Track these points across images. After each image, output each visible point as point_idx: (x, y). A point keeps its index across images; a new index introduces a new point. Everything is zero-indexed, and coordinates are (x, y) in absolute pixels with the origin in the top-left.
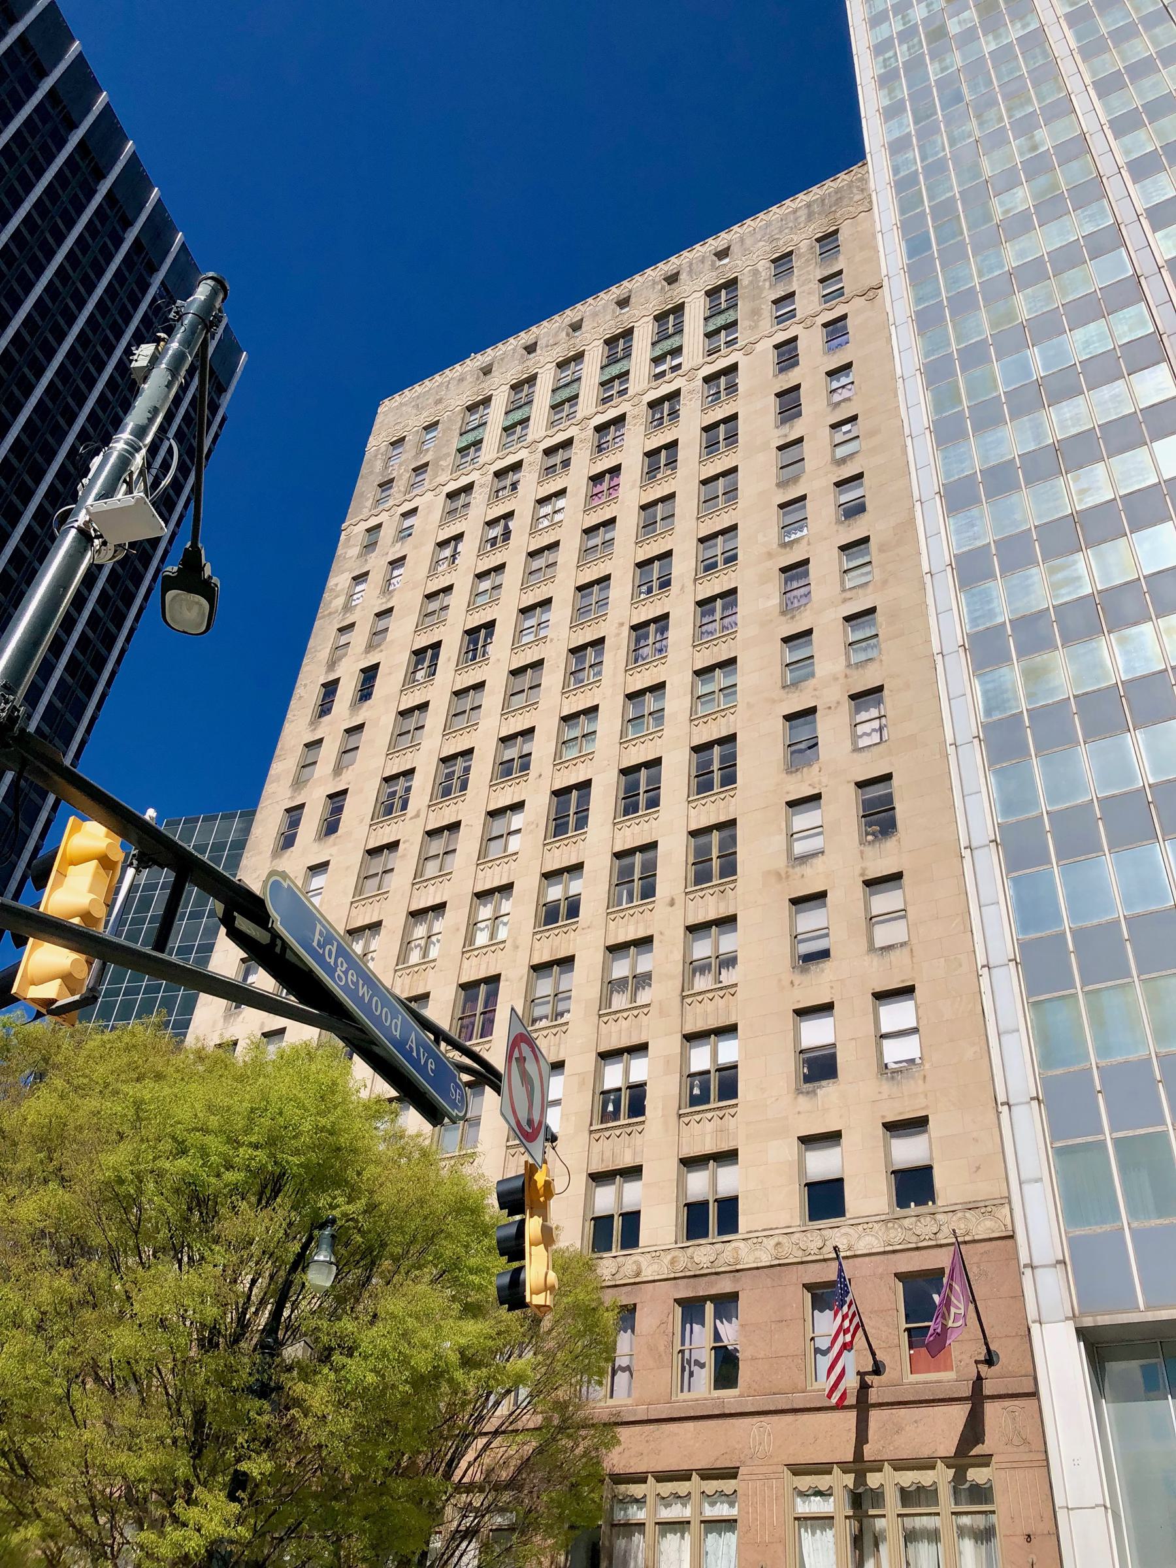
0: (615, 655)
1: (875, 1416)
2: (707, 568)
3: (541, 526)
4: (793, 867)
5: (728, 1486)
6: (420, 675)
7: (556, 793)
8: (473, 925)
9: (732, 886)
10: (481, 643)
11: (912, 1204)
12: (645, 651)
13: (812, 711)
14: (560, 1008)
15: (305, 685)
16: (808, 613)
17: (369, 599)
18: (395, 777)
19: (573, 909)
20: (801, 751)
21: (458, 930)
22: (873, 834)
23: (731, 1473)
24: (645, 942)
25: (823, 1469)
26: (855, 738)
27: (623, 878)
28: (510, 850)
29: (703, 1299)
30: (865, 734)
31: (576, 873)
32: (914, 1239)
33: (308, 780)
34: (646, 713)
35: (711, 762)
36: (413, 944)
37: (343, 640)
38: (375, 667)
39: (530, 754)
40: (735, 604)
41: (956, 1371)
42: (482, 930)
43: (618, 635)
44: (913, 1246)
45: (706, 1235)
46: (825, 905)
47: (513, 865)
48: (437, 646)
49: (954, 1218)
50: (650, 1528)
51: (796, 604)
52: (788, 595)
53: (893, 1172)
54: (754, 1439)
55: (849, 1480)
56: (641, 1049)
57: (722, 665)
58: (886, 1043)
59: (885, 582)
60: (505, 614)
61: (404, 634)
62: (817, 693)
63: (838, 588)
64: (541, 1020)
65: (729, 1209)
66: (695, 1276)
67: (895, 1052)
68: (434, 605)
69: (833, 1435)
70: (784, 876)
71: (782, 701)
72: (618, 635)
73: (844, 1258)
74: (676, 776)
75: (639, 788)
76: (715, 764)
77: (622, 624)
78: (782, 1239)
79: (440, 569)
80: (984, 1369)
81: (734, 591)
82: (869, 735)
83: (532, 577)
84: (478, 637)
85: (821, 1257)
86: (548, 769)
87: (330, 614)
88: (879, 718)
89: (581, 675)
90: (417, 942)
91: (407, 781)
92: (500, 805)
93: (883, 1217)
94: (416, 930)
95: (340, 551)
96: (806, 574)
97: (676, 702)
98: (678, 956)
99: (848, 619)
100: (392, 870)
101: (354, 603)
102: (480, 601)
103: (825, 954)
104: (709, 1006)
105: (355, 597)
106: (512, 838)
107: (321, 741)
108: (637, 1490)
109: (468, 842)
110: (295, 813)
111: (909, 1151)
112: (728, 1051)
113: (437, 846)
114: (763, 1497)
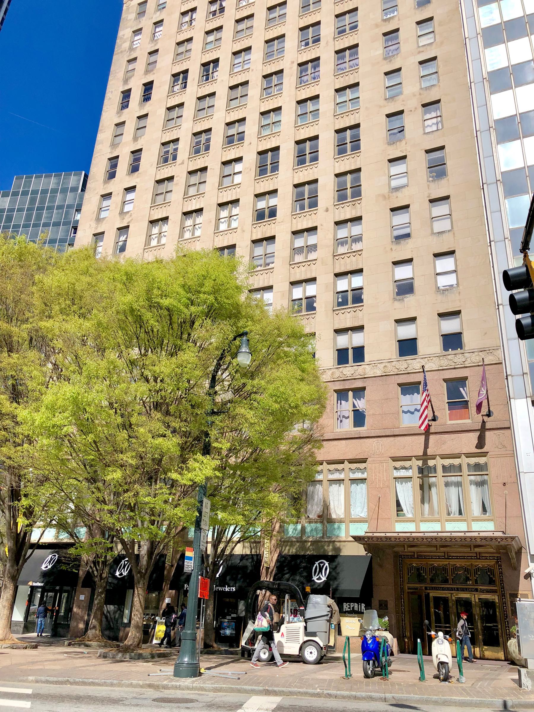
0: (254, 90)
1: (432, 437)
2: (339, 33)
3: (241, 5)
4: (392, 193)
5: (362, 466)
6: (176, 88)
7: (260, 153)
8: (183, 229)
9: (359, 202)
10: (211, 71)
11: (450, 350)
12: (305, 78)
13: (401, 112)
14: (268, 261)
15: (112, 92)
16: (399, 59)
17: (143, 45)
18: (168, 143)
19: (273, 213)
20: (394, 134)
21: (211, 222)
22: (432, 177)
23: (364, 461)
24: (313, 229)
25: (408, 458)
26: (424, 127)
27: (299, 199)
28: (235, 183)
29: (348, 390)
30: (428, 126)
31: (274, 195)
32: (453, 364)
33: (119, 143)
34: (308, 112)
35: (345, 138)
36: (185, 229)
37: (131, 67)
38: (151, 83)
39: (244, 132)
40: (318, 65)
41: (473, 419)
42: (223, 223)
43: (291, 68)
44: (453, 367)
45: (348, 363)
46: (361, 224)
47: (238, 190)
48: (186, 72)
49: (474, 355)
50: (325, 483)
51: (391, 54)
52: (387, 49)
53: (398, 341)
54: (375, 447)
55: (420, 463)
56: (313, 280)
57: (350, 87)
58: (439, 277)
59: (442, 43)
60: (224, 55)
61: (166, 66)
62: (404, 103)
63: (416, 46)
64: (258, 267)
65: (359, 353)
66: (344, 380)
67: (443, 281)
68: (182, 49)
69: (415, 445)
70: (387, 197)
71: (385, 106)
72: (291, 68)
73: (427, 371)
74: (327, 144)
75: (306, 150)
76: (349, 138)
77: (293, 62)
78: (386, 364)
79: (183, 28)
80: (486, 418)
81: (357, 46)
82: (431, 126)
83: (238, 35)
84: (209, 67)
85: (407, 372)
86: (255, 141)
87: (122, 52)
88: (437, 117)
89: (269, 90)
90: (188, 228)
91: (174, 145)
92: (228, 159)
93: (438, 355)
94: (186, 222)
95: (124, 15)
96: (397, 37)
97: (326, 105)
98: (331, 236)
99: (421, 63)
100: (171, 191)
101: (134, 47)
102: (209, 47)
103: (408, 236)
104: (348, 260)
105: (135, 43)
106: (236, 176)
107: (124, 123)
108: (320, 468)
109: (212, 177)
110: (114, 161)
111: (450, 326)
112: (357, 281)
113: (194, 179)
114: (379, 470)
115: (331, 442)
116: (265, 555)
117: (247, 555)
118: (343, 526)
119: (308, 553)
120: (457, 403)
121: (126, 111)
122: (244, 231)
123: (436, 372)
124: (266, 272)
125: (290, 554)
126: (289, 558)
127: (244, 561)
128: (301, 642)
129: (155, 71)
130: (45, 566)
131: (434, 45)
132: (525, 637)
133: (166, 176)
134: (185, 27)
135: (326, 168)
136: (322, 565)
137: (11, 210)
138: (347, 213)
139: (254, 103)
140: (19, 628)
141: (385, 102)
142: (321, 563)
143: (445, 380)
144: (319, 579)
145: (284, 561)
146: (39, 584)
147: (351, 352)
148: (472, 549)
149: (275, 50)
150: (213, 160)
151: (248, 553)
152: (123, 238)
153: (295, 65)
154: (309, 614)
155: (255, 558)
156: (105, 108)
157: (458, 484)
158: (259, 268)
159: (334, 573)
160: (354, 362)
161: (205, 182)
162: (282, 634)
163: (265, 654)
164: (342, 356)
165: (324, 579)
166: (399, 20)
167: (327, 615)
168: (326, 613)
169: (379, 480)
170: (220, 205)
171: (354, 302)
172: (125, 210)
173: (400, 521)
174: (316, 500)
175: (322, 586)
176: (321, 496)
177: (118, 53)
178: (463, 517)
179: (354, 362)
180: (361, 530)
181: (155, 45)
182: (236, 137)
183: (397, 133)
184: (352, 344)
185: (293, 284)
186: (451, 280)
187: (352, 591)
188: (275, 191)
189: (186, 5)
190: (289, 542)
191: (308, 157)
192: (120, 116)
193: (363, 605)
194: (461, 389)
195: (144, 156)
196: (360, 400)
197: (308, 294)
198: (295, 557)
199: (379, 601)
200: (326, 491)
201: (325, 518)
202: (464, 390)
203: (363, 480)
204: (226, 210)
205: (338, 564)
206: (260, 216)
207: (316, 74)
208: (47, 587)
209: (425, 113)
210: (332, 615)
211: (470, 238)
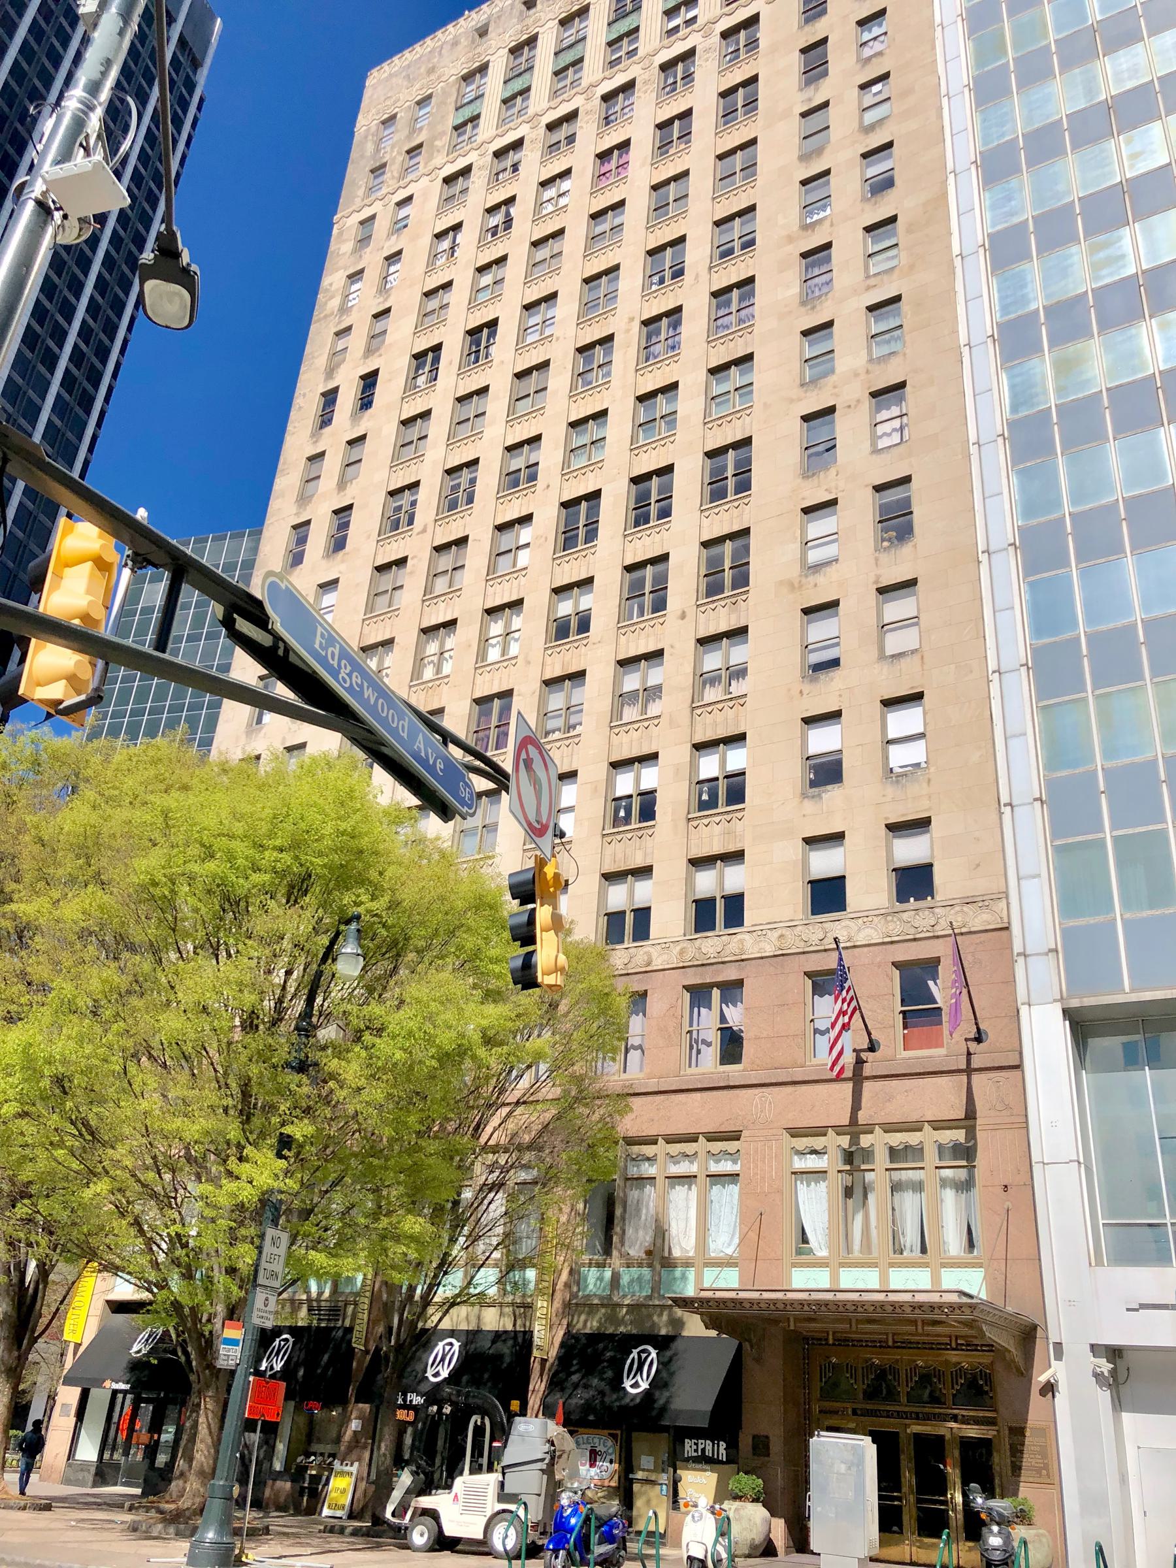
0: (625, 353)
1: (867, 1085)
2: (724, 255)
3: (545, 212)
4: (806, 576)
5: (731, 1146)
6: (421, 380)
7: (565, 505)
9: (744, 597)
10: (483, 344)
11: (912, 899)
13: (831, 410)
15: (304, 395)
16: (829, 303)
17: (365, 298)
19: (584, 625)
22: (889, 540)
25: (820, 1132)
26: (874, 438)
27: (634, 593)
28: (520, 565)
29: (711, 986)
30: (885, 434)
31: (587, 587)
32: (913, 931)
35: (724, 468)
36: (426, 661)
38: (375, 373)
40: (752, 294)
43: (628, 331)
44: (911, 937)
46: (837, 615)
48: (437, 348)
50: (660, 1181)
51: (817, 293)
53: (810, 882)
54: (756, 1106)
55: (845, 1141)
56: (651, 758)
59: (912, 267)
60: (508, 312)
61: (403, 337)
63: (862, 275)
64: (554, 732)
67: (900, 756)
69: (834, 1102)
70: (796, 585)
71: (800, 400)
72: (628, 331)
75: (650, 496)
76: (730, 468)
77: (632, 319)
78: (784, 931)
79: (438, 263)
80: (973, 1046)
82: (889, 435)
84: (481, 336)
85: (822, 948)
87: (326, 317)
89: (588, 376)
90: (430, 659)
91: (412, 495)
93: (882, 911)
94: (428, 647)
95: (333, 247)
96: (828, 259)
98: (689, 669)
99: (871, 309)
100: (402, 587)
101: (350, 304)
102: (482, 297)
103: (835, 663)
105: (351, 297)
107: (323, 454)
108: (649, 1150)
109: (476, 557)
111: (910, 851)
112: (736, 759)
113: (446, 561)
115: (673, 1097)
116: (536, 1334)
117: (506, 1332)
118: (691, 1274)
119: (622, 1329)
120: (919, 1011)
121: (327, 430)
122: (529, 663)
123: (877, 948)
124: (567, 742)
125: (588, 1331)
126: (583, 1341)
127: (499, 1345)
128: (489, 1514)
129: (382, 351)
131: (897, 271)
132: (819, 1509)
133: (393, 558)
134: (442, 261)
136: (643, 1356)
138: (721, 619)
139: (559, 403)
140: (86, 1474)
142: (644, 1351)
143: (895, 965)
145: (573, 1347)
147: (720, 906)
148: (920, 1327)
149: (736, 238)
150: (477, 523)
151: (510, 1327)
153: (636, 325)
155: (520, 1340)
156: (290, 428)
157: (918, 1187)
158: (557, 735)
159: (664, 1374)
160: (726, 927)
161: (463, 566)
162: (456, 1496)
163: (422, 1535)
164: (703, 915)
165: (644, 1385)
166: (832, 225)
167: (542, 1460)
168: (540, 1456)
169: (763, 1178)
170: (489, 612)
171: (730, 802)
173: (802, 1265)
174: (643, 1217)
175: (638, 1400)
176: (652, 1211)
177: (319, 321)
178: (926, 1258)
179: (726, 927)
180: (725, 1282)
181: (386, 300)
182: (523, 475)
183: (823, 453)
185: (617, 765)
186: (914, 753)
187: (693, 1414)
188: (589, 581)
189: (444, 219)
190: (588, 1307)
191: (731, 483)
192: (316, 442)
193: (723, 1445)
194: (931, 983)
195: (355, 517)
196: (735, 1006)
197: (645, 786)
198: (595, 1338)
199: (754, 1437)
200: (664, 1200)
201: (659, 1258)
202: (936, 984)
203: (733, 1177)
204: (500, 621)
205: (675, 1354)
206: (560, 630)
207: (677, 338)
209: (878, 409)
210: (553, 1458)
211: (953, 666)
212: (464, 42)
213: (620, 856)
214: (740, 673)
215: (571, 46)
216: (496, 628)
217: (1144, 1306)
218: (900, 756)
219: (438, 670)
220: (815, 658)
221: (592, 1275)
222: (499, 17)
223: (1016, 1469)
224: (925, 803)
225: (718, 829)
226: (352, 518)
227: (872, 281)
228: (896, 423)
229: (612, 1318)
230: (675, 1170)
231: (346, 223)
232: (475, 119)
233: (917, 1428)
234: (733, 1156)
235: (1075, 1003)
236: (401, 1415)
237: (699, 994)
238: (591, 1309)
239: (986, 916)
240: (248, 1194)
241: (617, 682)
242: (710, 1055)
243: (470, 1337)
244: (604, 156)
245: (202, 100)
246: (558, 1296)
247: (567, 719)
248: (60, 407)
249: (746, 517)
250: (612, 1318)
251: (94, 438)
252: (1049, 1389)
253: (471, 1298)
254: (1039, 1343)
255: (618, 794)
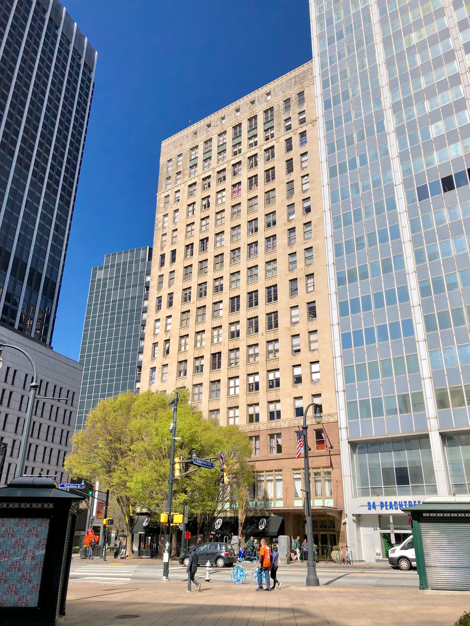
5: (280, 473)
16: (295, 246)
17: (169, 226)
24: (257, 345)
25: (299, 469)
27: (250, 325)
35: (271, 291)
40: (276, 239)
43: (244, 247)
48: (192, 244)
63: (303, 239)
72: (244, 247)
80: (330, 449)
87: (158, 229)
89: (235, 259)
95: (158, 205)
98: (265, 350)
99: (305, 249)
108: (262, 474)
112: (278, 374)
121: (163, 268)
130: (145, 524)
135: (262, 310)
137: (105, 279)
141: (289, 272)
144: (262, 527)
146: (143, 533)
151: (233, 516)
152: (167, 346)
153: (246, 245)
154: (232, 543)
157: (320, 481)
165: (263, 527)
172: (168, 329)
180: (279, 505)
184: (276, 409)
198: (252, 517)
200: (266, 485)
201: (266, 499)
208: (148, 534)
212: (190, 137)
213: (251, 400)
214: (277, 351)
215: (222, 145)
216: (215, 333)
217: (362, 506)
218: (315, 377)
219: (201, 345)
220: (295, 348)
221: (251, 503)
222: (200, 129)
223: (338, 540)
224: (320, 390)
225: (274, 394)
226: (174, 296)
227: (305, 241)
228: (312, 284)
229: (256, 513)
230: (268, 478)
231: (160, 196)
232: (196, 165)
233: (321, 533)
234: (281, 475)
235: (350, 440)
236: (211, 536)
237: (272, 436)
238: (251, 511)
239: (333, 419)
240: (182, 501)
241: (248, 351)
242: (275, 450)
243: (224, 518)
244: (234, 186)
245: (94, 84)
246: (243, 508)
247: (235, 361)
248: (60, 207)
249: (277, 308)
250: (256, 513)
251: (72, 215)
252: (345, 523)
253: (225, 508)
254: (343, 514)
255: (250, 383)
